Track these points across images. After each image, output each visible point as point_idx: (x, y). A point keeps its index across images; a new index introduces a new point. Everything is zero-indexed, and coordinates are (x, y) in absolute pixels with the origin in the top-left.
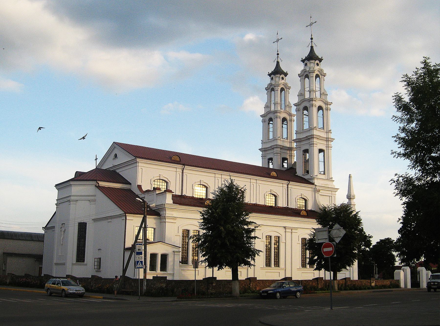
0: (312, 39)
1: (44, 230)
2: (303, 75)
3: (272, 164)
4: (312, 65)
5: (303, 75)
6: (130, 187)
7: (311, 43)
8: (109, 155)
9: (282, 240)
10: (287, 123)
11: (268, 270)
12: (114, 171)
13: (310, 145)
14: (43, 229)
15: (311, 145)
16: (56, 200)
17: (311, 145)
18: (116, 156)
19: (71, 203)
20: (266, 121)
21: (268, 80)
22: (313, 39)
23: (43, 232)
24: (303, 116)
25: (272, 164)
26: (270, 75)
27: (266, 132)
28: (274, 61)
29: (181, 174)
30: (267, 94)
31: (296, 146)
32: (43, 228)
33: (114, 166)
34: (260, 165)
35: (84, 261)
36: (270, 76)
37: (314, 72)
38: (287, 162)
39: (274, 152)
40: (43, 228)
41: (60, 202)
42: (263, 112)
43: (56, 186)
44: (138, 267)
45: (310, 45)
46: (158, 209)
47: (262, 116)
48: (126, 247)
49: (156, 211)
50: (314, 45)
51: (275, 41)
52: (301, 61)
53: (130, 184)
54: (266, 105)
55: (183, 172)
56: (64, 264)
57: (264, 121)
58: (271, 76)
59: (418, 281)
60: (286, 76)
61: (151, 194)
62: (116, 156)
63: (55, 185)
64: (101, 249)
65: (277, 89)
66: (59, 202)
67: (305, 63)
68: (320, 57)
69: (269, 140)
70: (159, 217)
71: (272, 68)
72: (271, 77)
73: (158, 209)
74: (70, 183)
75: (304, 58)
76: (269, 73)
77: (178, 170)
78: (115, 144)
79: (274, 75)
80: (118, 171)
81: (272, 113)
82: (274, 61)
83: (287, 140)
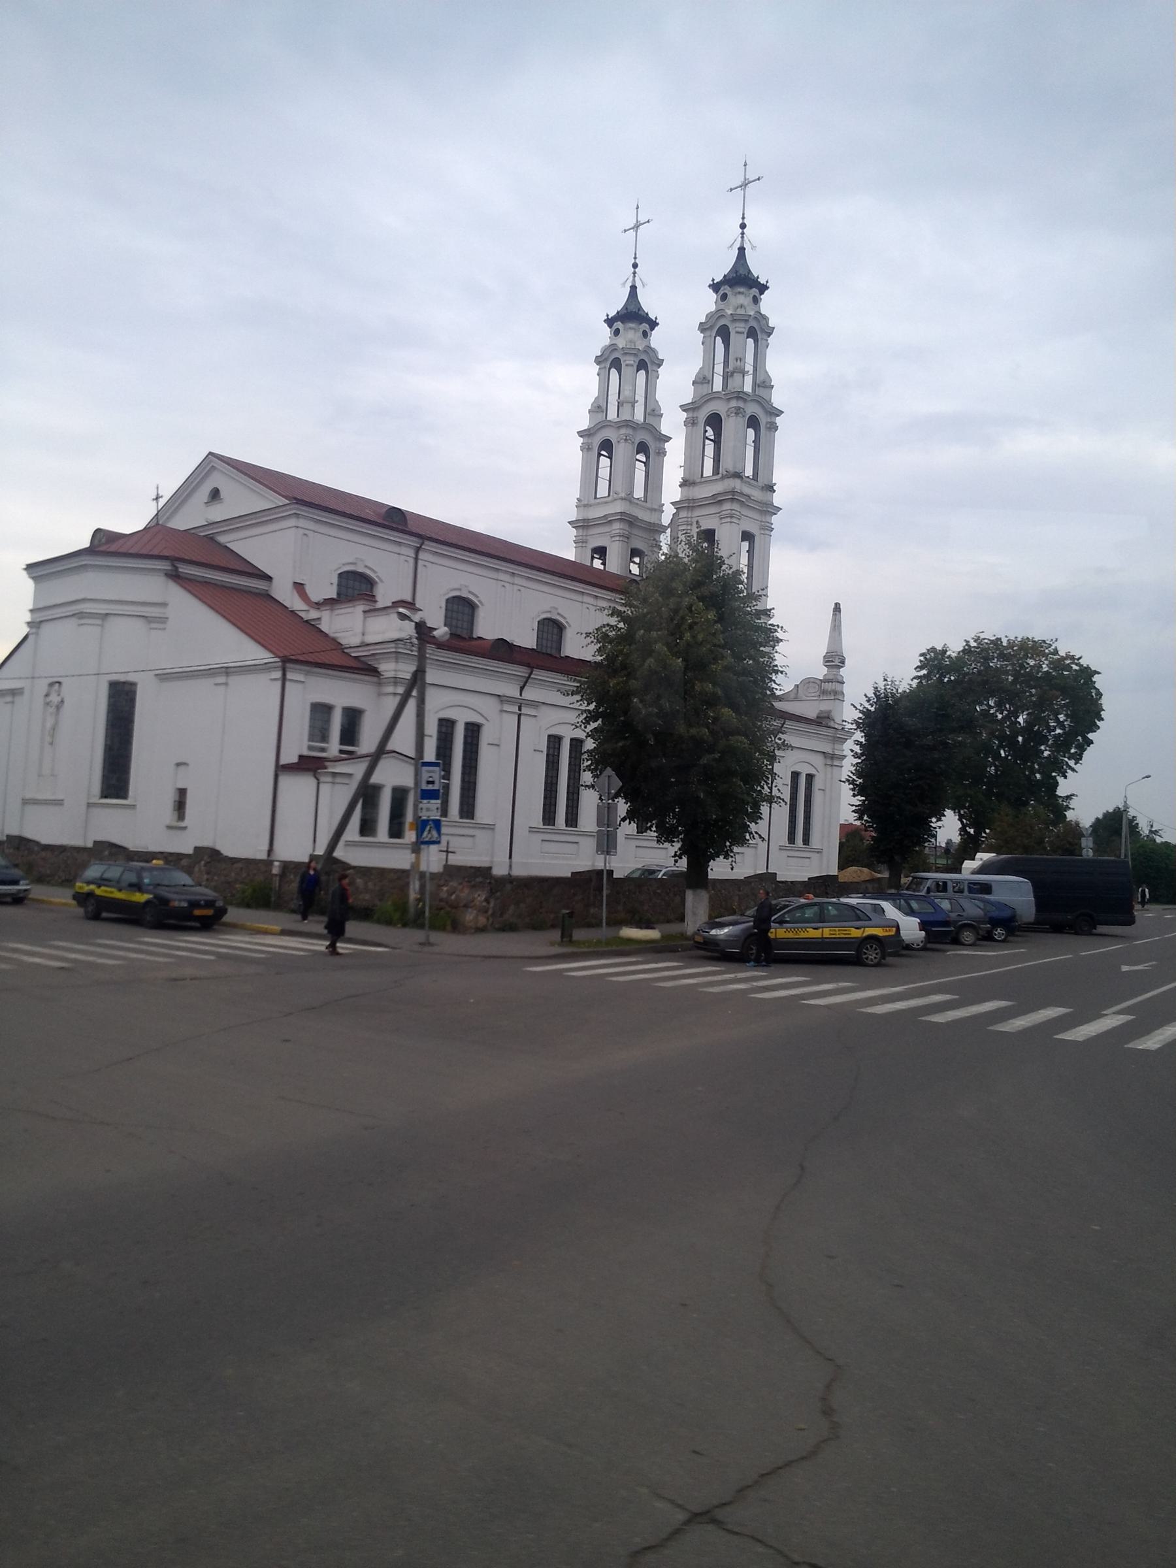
0: (635, 266)
2: (711, 328)
3: (602, 564)
4: (740, 299)
5: (711, 328)
7: (631, 278)
8: (189, 495)
10: (648, 457)
11: (642, 841)
12: (211, 539)
13: (612, 537)
15: (724, 518)
17: (724, 518)
18: (215, 494)
20: (592, 448)
21: (604, 335)
22: (747, 225)
24: (704, 442)
27: (590, 476)
30: (703, 344)
31: (575, 536)
34: (573, 560)
35: (124, 796)
36: (610, 327)
38: (638, 562)
39: (614, 532)
42: (585, 424)
43: (30, 567)
45: (738, 245)
46: (373, 654)
47: (581, 434)
48: (283, 762)
51: (630, 227)
52: (710, 286)
53: (269, 578)
54: (595, 405)
55: (416, 559)
57: (586, 448)
58: (722, 289)
62: (215, 494)
66: (40, 616)
67: (721, 292)
69: (598, 501)
70: (375, 679)
71: (723, 267)
72: (721, 292)
75: (718, 279)
78: (213, 459)
80: (222, 539)
81: (612, 426)
83: (644, 504)
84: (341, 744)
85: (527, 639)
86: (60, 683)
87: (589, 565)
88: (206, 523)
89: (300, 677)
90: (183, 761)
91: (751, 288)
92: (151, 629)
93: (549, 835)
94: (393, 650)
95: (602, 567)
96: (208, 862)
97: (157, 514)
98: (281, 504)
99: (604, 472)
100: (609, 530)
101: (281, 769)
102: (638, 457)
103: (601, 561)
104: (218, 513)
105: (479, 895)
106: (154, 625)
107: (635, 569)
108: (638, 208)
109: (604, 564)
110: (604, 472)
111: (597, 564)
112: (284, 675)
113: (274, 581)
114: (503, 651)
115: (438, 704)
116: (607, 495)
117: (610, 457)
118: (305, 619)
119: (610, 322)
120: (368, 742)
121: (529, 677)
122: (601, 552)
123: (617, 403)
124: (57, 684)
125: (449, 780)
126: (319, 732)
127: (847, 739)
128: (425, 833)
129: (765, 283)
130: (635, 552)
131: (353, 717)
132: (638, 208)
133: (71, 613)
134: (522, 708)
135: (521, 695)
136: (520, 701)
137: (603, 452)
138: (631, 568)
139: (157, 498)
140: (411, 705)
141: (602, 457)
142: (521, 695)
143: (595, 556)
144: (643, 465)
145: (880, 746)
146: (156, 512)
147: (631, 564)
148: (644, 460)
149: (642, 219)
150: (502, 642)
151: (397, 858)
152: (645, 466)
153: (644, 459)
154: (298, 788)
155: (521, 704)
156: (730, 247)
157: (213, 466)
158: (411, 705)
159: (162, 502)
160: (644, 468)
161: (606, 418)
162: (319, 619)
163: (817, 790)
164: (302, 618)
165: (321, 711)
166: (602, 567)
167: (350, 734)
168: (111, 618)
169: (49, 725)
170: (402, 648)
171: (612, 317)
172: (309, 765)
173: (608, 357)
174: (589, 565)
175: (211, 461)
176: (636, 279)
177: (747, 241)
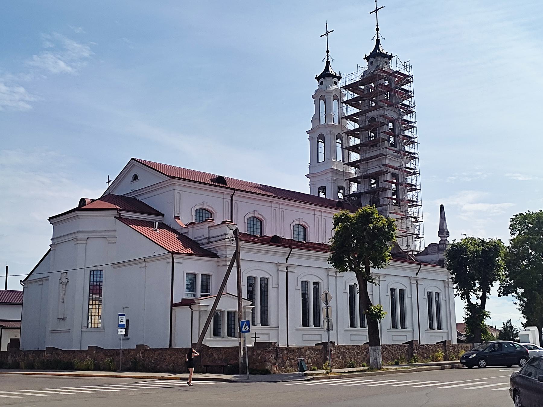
0: (377, 29)
1: (23, 284)
3: (324, 195)
6: (162, 220)
7: (326, 57)
9: (407, 294)
10: (342, 141)
12: (134, 199)
14: (21, 284)
16: (51, 239)
18: (136, 178)
19: (79, 242)
23: (21, 288)
25: (324, 195)
26: (318, 78)
28: (323, 60)
29: (230, 201)
32: (21, 281)
33: (133, 192)
34: (309, 194)
36: (318, 81)
37: (332, 93)
38: (342, 192)
40: (21, 281)
41: (56, 242)
43: (50, 219)
44: (244, 330)
45: (376, 38)
48: (174, 302)
49: (209, 251)
50: (330, 60)
53: (163, 215)
55: (232, 200)
56: (69, 331)
58: (370, 59)
59: (19, 342)
60: (339, 80)
61: (199, 228)
62: (136, 178)
63: (49, 219)
64: (128, 307)
65: (329, 96)
67: (370, 61)
68: (389, 54)
73: (214, 247)
74: (77, 213)
76: (316, 76)
77: (225, 196)
79: (323, 78)
80: (139, 198)
82: (323, 60)
84: (201, 292)
85: (288, 235)
86: (66, 273)
87: (318, 196)
88: (132, 191)
89: (181, 261)
90: (126, 306)
91: (384, 58)
92: (109, 243)
93: (306, 331)
94: (224, 244)
95: (324, 196)
96: (143, 352)
97: (109, 188)
98: (167, 180)
99: (321, 150)
100: (326, 178)
101: (173, 305)
102: (337, 141)
103: (324, 193)
104: (137, 186)
105: (271, 356)
106: (110, 242)
107: (340, 196)
108: (327, 25)
109: (325, 194)
110: (321, 150)
111: (322, 195)
112: (173, 260)
113: (165, 216)
114: (276, 241)
115: (247, 270)
116: (324, 161)
117: (324, 142)
118: (181, 233)
119: (318, 78)
120: (215, 287)
121: (290, 253)
122: (323, 189)
123: (325, 116)
124: (65, 273)
125: (255, 306)
126: (191, 287)
127: (102, 199)
128: (243, 328)
129: (391, 55)
130: (339, 188)
131: (206, 279)
132: (327, 25)
133: (71, 239)
134: (288, 269)
135: (287, 262)
136: (287, 265)
137: (320, 140)
138: (338, 195)
139: (109, 182)
140: (234, 270)
141: (319, 143)
142: (287, 262)
143: (320, 191)
144: (340, 144)
145: (380, 256)
146: (108, 187)
147: (339, 193)
148: (340, 142)
149: (329, 30)
150: (275, 237)
151: (232, 342)
152: (341, 145)
153: (340, 142)
154: (183, 313)
155: (379, 276)
156: (372, 39)
157: (134, 164)
158: (234, 270)
159: (111, 183)
160: (341, 146)
161: (320, 124)
162: (187, 232)
163: (442, 300)
164: (180, 233)
165: (192, 278)
166: (324, 196)
167: (206, 288)
168: (89, 239)
169: (62, 294)
170: (228, 243)
171: (319, 76)
172: (187, 303)
173: (318, 95)
174: (318, 196)
175: (133, 162)
176: (329, 57)
177: (380, 36)
